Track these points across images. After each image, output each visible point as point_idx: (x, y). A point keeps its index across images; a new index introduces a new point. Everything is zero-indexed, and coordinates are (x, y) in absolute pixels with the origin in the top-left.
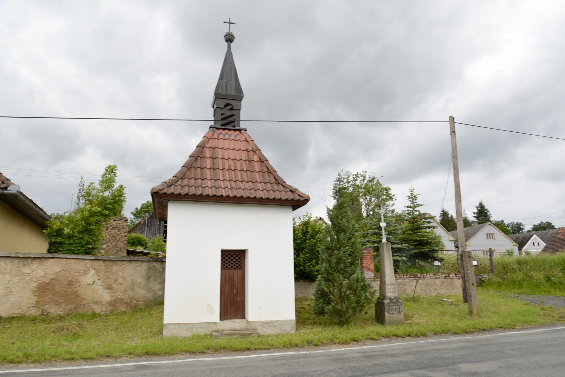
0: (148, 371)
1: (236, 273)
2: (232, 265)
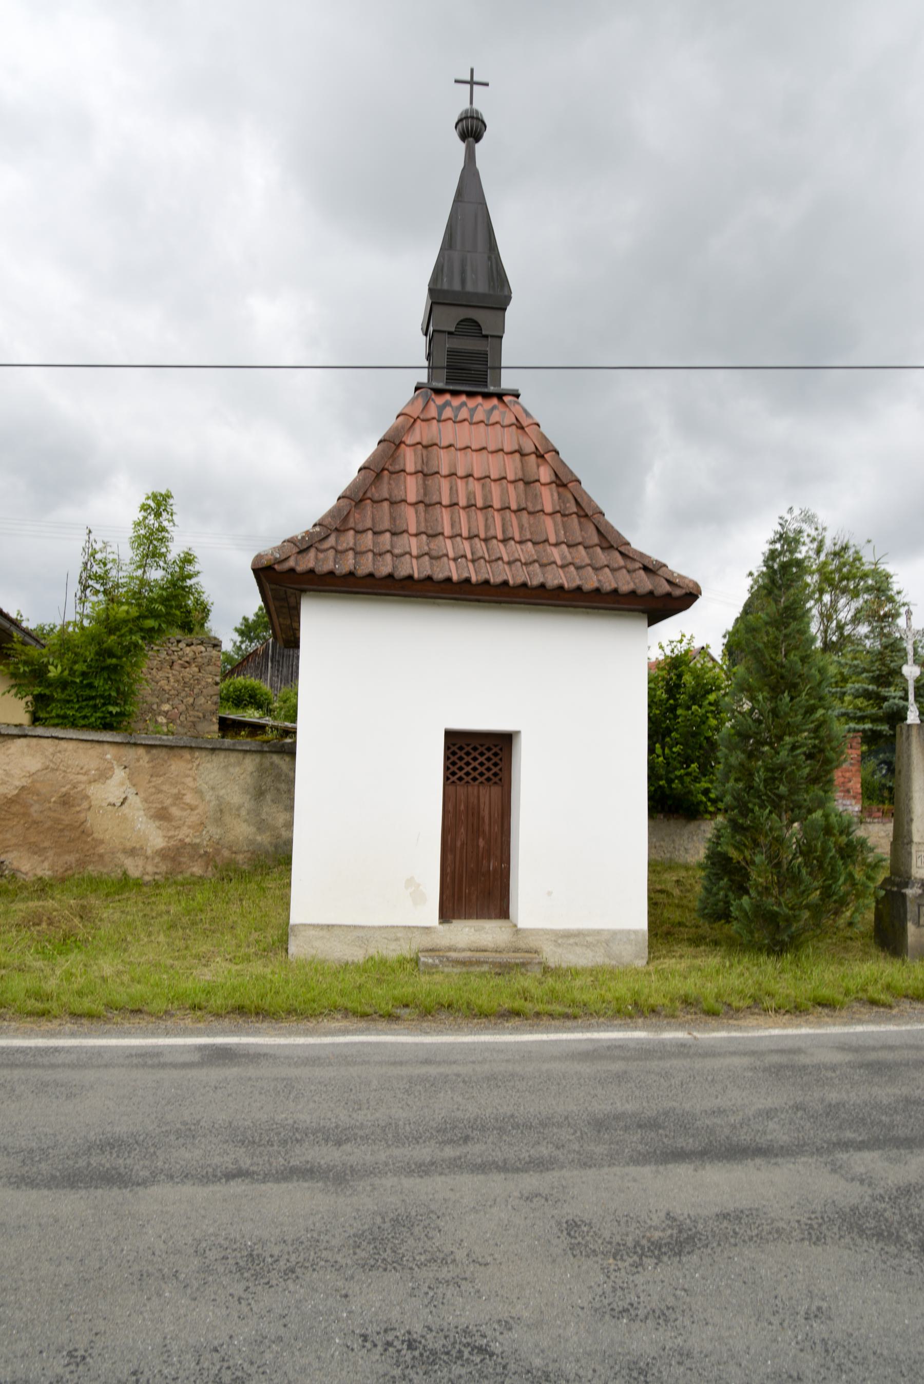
0: (232, 1072)
1: (487, 795)
2: (475, 774)
